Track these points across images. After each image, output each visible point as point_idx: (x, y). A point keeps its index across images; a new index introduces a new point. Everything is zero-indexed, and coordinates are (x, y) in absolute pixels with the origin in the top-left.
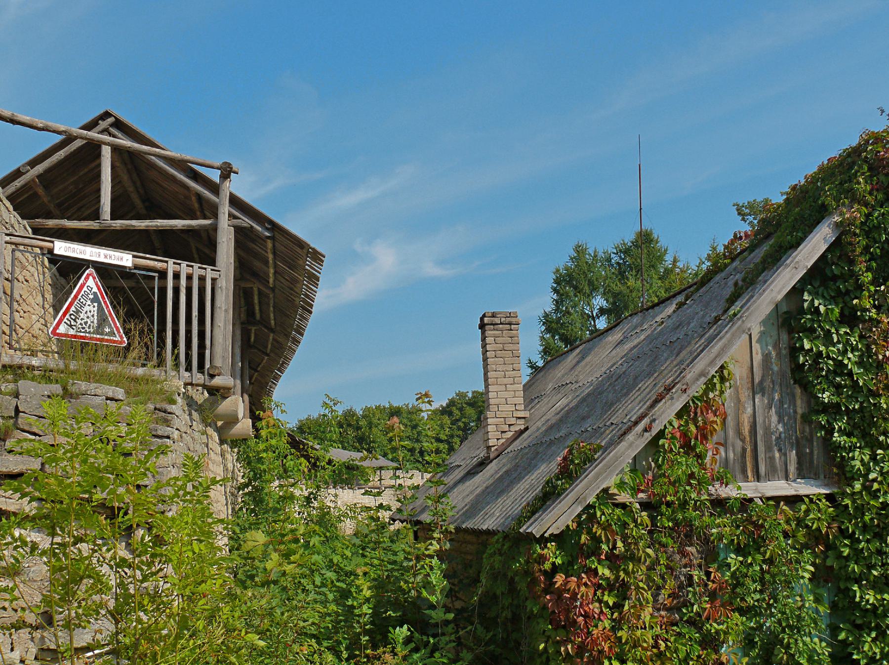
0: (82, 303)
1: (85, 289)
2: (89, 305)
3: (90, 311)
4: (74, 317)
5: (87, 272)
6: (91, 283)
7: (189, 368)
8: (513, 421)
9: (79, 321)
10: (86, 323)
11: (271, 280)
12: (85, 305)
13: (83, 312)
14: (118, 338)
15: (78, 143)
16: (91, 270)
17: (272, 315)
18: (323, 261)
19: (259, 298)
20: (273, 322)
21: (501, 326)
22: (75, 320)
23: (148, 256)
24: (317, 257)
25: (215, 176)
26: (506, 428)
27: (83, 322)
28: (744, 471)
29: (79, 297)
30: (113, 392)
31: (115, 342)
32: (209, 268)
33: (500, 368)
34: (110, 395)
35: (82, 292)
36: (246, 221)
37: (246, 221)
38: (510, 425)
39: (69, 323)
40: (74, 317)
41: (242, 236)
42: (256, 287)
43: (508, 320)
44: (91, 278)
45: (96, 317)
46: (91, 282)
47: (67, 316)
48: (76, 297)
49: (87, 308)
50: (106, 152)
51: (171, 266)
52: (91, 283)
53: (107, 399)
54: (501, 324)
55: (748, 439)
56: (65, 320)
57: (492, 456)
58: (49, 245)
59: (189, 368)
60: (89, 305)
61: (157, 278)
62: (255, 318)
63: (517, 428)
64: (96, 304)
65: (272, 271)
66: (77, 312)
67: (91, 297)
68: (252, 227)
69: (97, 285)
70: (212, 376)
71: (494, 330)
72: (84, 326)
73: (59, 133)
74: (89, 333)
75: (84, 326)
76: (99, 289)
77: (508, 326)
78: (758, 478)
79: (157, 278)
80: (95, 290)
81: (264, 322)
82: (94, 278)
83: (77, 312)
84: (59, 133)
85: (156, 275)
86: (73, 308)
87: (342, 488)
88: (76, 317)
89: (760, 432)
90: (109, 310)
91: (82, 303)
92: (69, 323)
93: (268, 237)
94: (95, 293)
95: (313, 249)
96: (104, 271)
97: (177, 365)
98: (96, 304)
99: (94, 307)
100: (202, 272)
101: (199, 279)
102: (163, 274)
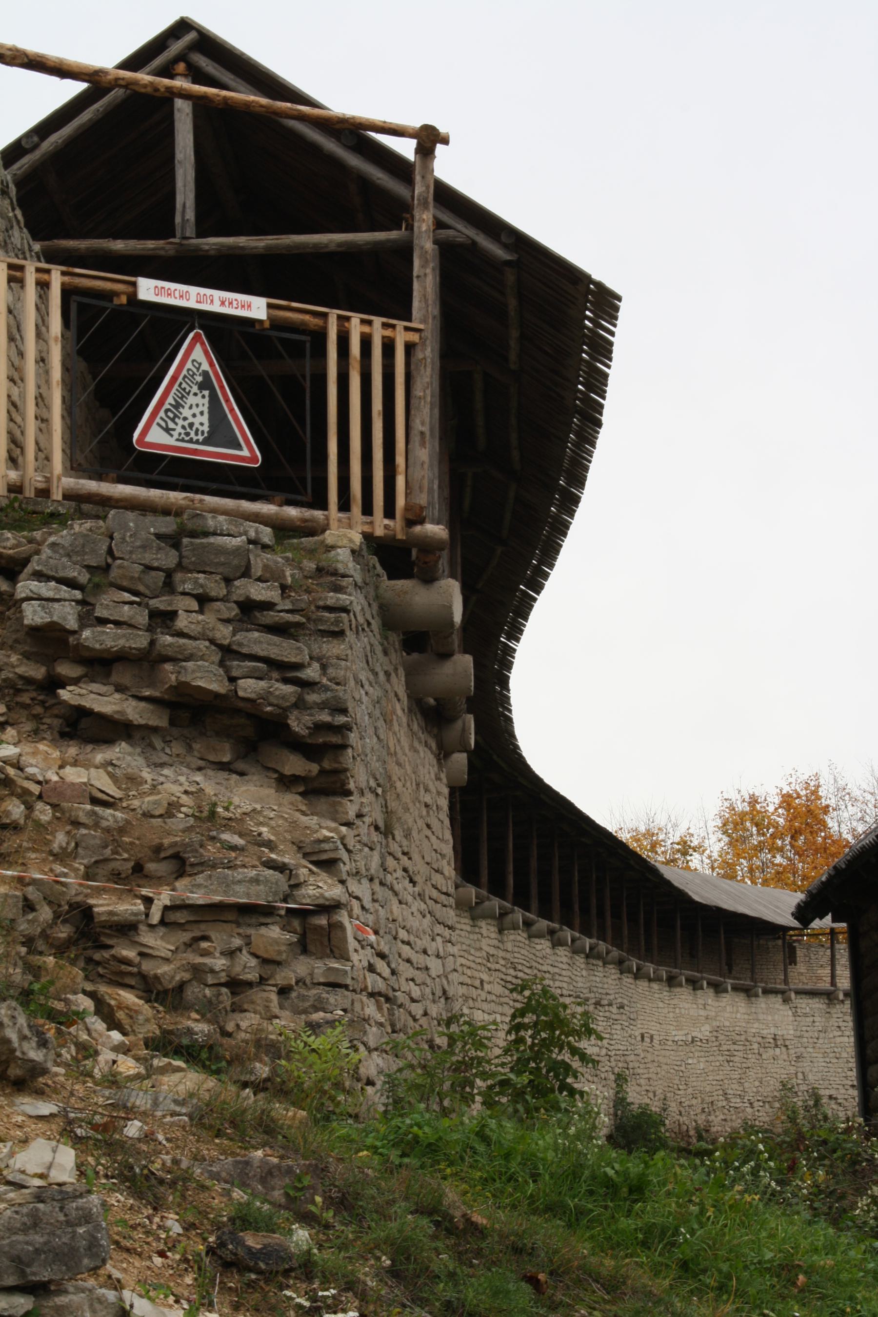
0: (184, 389)
1: (189, 365)
2: (195, 394)
3: (197, 405)
4: (171, 415)
5: (191, 335)
7: (368, 509)
9: (180, 422)
10: (191, 425)
11: (513, 356)
12: (188, 394)
13: (187, 406)
14: (245, 453)
15: (116, 94)
20: (515, 454)
22: (173, 420)
23: (295, 305)
24: (619, 299)
25: (406, 148)
27: (186, 423)
29: (180, 379)
30: (257, 532)
31: (243, 459)
32: (400, 324)
35: (184, 372)
36: (463, 231)
37: (463, 231)
39: (163, 424)
40: (171, 415)
45: (206, 415)
46: (198, 353)
47: (162, 414)
48: (174, 379)
49: (191, 400)
50: (183, 110)
56: (158, 420)
59: (368, 509)
60: (195, 394)
61: (308, 345)
64: (206, 393)
65: (515, 334)
66: (177, 406)
67: (199, 379)
68: (474, 243)
70: (410, 523)
72: (188, 430)
73: (61, 70)
74: (197, 442)
75: (188, 430)
76: (211, 364)
79: (308, 345)
80: (205, 366)
82: (203, 344)
84: (61, 70)
85: (308, 338)
86: (170, 400)
88: (176, 416)
91: (184, 389)
92: (163, 424)
93: (508, 263)
94: (205, 374)
97: (345, 505)
98: (206, 393)
99: (203, 397)
100: (388, 333)
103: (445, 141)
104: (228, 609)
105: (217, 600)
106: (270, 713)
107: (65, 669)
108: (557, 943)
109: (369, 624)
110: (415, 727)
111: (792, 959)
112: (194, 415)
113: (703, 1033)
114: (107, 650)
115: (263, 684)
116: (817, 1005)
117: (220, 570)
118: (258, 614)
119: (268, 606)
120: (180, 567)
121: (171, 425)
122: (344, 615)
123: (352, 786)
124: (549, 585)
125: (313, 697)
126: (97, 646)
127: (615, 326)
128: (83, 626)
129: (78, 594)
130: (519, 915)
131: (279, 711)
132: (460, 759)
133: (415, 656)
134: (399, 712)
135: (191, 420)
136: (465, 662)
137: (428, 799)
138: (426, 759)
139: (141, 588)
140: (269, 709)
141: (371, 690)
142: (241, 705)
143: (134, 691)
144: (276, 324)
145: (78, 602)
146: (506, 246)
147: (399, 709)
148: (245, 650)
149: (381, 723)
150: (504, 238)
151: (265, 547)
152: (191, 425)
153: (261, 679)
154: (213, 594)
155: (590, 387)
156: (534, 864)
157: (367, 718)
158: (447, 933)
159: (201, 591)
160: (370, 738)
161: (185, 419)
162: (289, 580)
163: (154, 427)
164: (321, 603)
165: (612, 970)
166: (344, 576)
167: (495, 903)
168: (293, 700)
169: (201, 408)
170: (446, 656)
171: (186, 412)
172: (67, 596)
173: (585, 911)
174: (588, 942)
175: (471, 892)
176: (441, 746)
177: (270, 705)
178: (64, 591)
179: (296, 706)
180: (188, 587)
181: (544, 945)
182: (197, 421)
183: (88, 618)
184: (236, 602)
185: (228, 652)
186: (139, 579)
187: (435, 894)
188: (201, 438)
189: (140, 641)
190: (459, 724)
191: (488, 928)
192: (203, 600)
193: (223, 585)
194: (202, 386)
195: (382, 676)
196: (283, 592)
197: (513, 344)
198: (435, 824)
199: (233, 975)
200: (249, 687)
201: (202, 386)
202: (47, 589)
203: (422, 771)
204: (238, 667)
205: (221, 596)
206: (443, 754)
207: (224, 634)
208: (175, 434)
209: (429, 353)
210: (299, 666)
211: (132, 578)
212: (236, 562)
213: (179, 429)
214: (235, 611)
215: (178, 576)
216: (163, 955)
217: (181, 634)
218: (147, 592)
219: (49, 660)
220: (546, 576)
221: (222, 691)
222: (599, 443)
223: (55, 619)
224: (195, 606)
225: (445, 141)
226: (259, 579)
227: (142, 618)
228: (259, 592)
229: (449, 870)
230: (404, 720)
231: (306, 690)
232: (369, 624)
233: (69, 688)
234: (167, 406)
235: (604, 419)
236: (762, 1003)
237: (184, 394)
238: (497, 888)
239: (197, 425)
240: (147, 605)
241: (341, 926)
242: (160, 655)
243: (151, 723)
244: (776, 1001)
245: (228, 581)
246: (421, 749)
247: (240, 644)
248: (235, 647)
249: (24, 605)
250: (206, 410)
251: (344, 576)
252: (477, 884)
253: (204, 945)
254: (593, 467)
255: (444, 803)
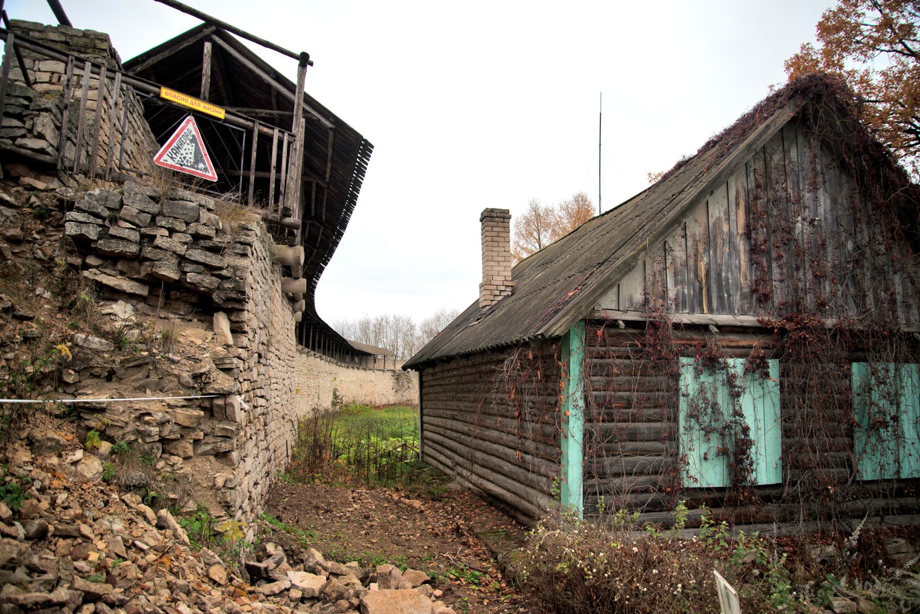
1: (186, 131)
5: (188, 118)
6: (189, 127)
8: (503, 288)
10: (185, 158)
11: (328, 176)
16: (190, 118)
17: (324, 213)
18: (370, 156)
19: (316, 195)
21: (497, 219)
22: (175, 154)
24: (372, 147)
26: (497, 293)
27: (182, 156)
28: (701, 305)
29: (181, 136)
30: (206, 201)
33: (495, 249)
34: (203, 203)
35: (183, 133)
38: (501, 291)
41: (311, 124)
42: (315, 180)
43: (502, 215)
44: (191, 123)
45: (193, 155)
47: (170, 150)
48: (178, 135)
49: (186, 146)
51: (258, 128)
52: (189, 127)
53: (200, 205)
54: (497, 217)
55: (704, 281)
56: (168, 153)
57: (537, 237)
58: (156, 89)
62: (310, 214)
63: (506, 294)
64: (194, 145)
66: (178, 148)
67: (191, 138)
68: (319, 120)
69: (195, 129)
71: (491, 221)
74: (187, 166)
77: (502, 220)
78: (711, 311)
79: (245, 134)
80: (194, 133)
81: (318, 218)
82: (193, 124)
83: (178, 148)
86: (175, 144)
87: (353, 367)
89: (713, 275)
90: (204, 150)
93: (331, 129)
94: (193, 136)
95: (366, 141)
96: (203, 120)
98: (194, 145)
101: (279, 140)
102: (250, 132)
103: (311, 64)
104: (186, 237)
105: (180, 232)
106: (204, 291)
107: (91, 260)
108: (322, 359)
109: (265, 259)
110: (285, 303)
111: (375, 362)
112: (187, 154)
113: (354, 379)
114: (112, 252)
115: (200, 276)
116: (381, 373)
117: (183, 217)
118: (202, 241)
119: (209, 238)
120: (161, 213)
121: (174, 156)
122: (249, 247)
123: (246, 328)
124: (329, 263)
125: (227, 285)
126: (107, 249)
127: (368, 160)
128: (100, 238)
129: (100, 221)
130: (312, 353)
131: (208, 290)
132: (299, 314)
133: (286, 278)
134: (278, 297)
135: (185, 155)
136: (303, 282)
137: (288, 327)
138: (288, 313)
139: (137, 221)
140: (203, 289)
141: (263, 286)
142: (188, 286)
143: (129, 275)
144: (226, 120)
145: (100, 226)
146: (331, 122)
147: (278, 296)
148: (192, 258)
149: (268, 300)
150: (330, 119)
151: (209, 210)
152: (185, 158)
153: (200, 273)
154: (177, 228)
155: (359, 172)
156: (317, 339)
157: (260, 297)
158: (292, 370)
159: (170, 226)
160: (261, 305)
161: (182, 154)
162: (221, 227)
163: (166, 155)
164: (237, 240)
165: (334, 365)
166: (251, 230)
167: (306, 350)
168: (216, 285)
169: (190, 151)
170: (297, 278)
171: (182, 151)
172: (93, 222)
173: (329, 350)
174: (329, 359)
175: (300, 347)
176: (293, 309)
177: (204, 287)
178: (92, 219)
179: (218, 288)
180: (163, 223)
181: (318, 360)
182: (188, 157)
183: (104, 234)
184: (190, 234)
185: (182, 259)
186: (136, 216)
187: (289, 358)
188: (189, 164)
189: (134, 249)
190: (300, 303)
191: (304, 356)
192: (172, 231)
193: (184, 225)
194: (191, 141)
195: (270, 281)
196: (217, 232)
197: (328, 170)
198: (290, 335)
199: (163, 436)
200: (191, 277)
201: (191, 141)
202: (80, 217)
203: (286, 318)
204: (188, 268)
205: (183, 230)
206: (294, 311)
207: (182, 250)
208: (176, 160)
209: (299, 143)
210: (221, 269)
211: (132, 215)
212: (192, 214)
213: (178, 158)
214: (189, 238)
215: (158, 219)
216: (119, 425)
217: (157, 247)
218: (141, 225)
219: (84, 256)
220: (329, 260)
221: (177, 278)
222: (354, 212)
223: (83, 232)
224: (166, 233)
225: (311, 64)
226: (204, 224)
227: (135, 236)
228: (204, 231)
229: (294, 341)
230: (280, 300)
231: (224, 281)
232: (265, 259)
233: (90, 270)
234: (172, 147)
235: (358, 202)
236: (368, 372)
237: (182, 143)
238: (307, 346)
239: (188, 158)
240: (139, 231)
241: (232, 405)
242: (143, 257)
243: (137, 292)
244: (371, 371)
245: (187, 224)
246: (286, 310)
247: (190, 255)
248: (187, 256)
249: (67, 224)
250: (193, 152)
251: (251, 230)
252: (302, 344)
253: (147, 418)
254: (350, 222)
255: (294, 328)
